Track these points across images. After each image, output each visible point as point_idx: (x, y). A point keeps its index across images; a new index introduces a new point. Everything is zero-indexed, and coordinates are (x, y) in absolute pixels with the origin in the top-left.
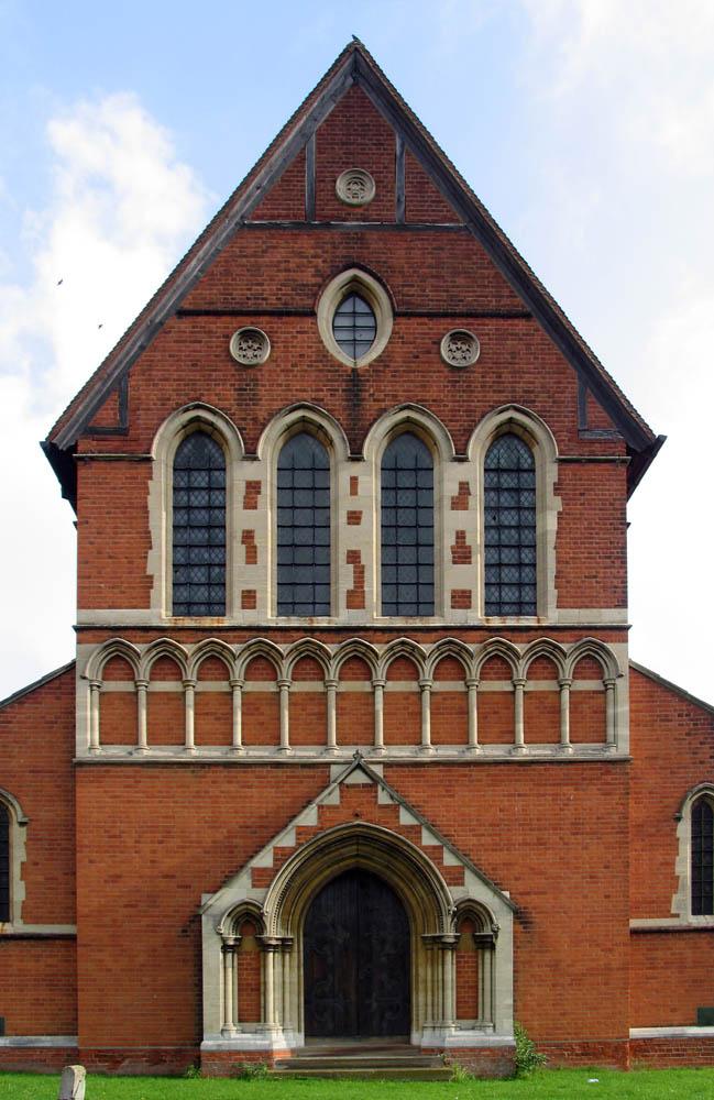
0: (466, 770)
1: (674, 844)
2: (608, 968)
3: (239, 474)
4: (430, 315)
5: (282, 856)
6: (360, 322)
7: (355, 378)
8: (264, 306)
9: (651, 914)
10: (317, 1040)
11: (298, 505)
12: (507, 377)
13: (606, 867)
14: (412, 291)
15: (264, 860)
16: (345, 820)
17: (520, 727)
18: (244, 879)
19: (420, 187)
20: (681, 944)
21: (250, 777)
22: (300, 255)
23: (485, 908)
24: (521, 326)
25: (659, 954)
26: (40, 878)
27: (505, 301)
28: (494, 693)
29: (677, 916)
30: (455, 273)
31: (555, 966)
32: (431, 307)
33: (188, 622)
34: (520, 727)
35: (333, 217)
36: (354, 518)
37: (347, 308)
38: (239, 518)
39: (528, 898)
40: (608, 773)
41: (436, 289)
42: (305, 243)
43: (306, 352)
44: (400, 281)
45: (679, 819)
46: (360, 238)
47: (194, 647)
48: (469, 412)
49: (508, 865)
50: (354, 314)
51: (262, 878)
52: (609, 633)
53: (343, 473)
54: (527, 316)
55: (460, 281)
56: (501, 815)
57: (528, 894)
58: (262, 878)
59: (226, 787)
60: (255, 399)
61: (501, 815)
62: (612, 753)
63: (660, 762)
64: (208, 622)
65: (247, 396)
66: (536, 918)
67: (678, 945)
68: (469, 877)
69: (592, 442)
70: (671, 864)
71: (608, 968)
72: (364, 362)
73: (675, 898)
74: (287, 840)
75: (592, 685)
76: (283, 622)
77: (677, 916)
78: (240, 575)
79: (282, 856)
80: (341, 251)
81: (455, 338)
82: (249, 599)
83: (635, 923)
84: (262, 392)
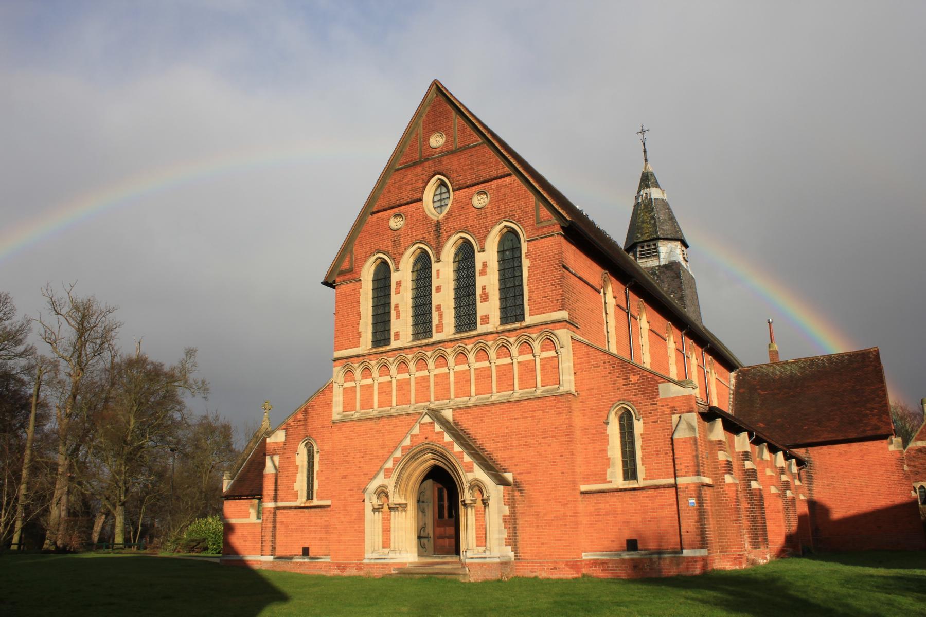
0: (489, 408)
2: (565, 516)
3: (479, 258)
4: (467, 187)
5: (396, 461)
6: (444, 196)
8: (403, 202)
9: (596, 482)
11: (661, 236)
12: (502, 206)
15: (389, 465)
16: (421, 440)
17: (516, 381)
18: (381, 475)
19: (463, 131)
21: (397, 422)
24: (508, 179)
25: (602, 506)
26: (323, 478)
29: (610, 482)
30: (478, 165)
31: (537, 514)
33: (508, 327)
34: (516, 381)
37: (438, 192)
38: (480, 281)
39: (523, 476)
44: (455, 175)
47: (515, 338)
49: (511, 458)
50: (441, 194)
51: (388, 473)
54: (509, 175)
55: (480, 168)
58: (388, 473)
59: (388, 427)
62: (562, 389)
63: (595, 391)
64: (516, 325)
65: (396, 243)
66: (526, 487)
67: (613, 499)
71: (565, 516)
74: (398, 454)
75: (552, 353)
77: (610, 482)
78: (482, 309)
79: (396, 461)
80: (433, 169)
81: (479, 193)
82: (486, 320)
83: (584, 488)
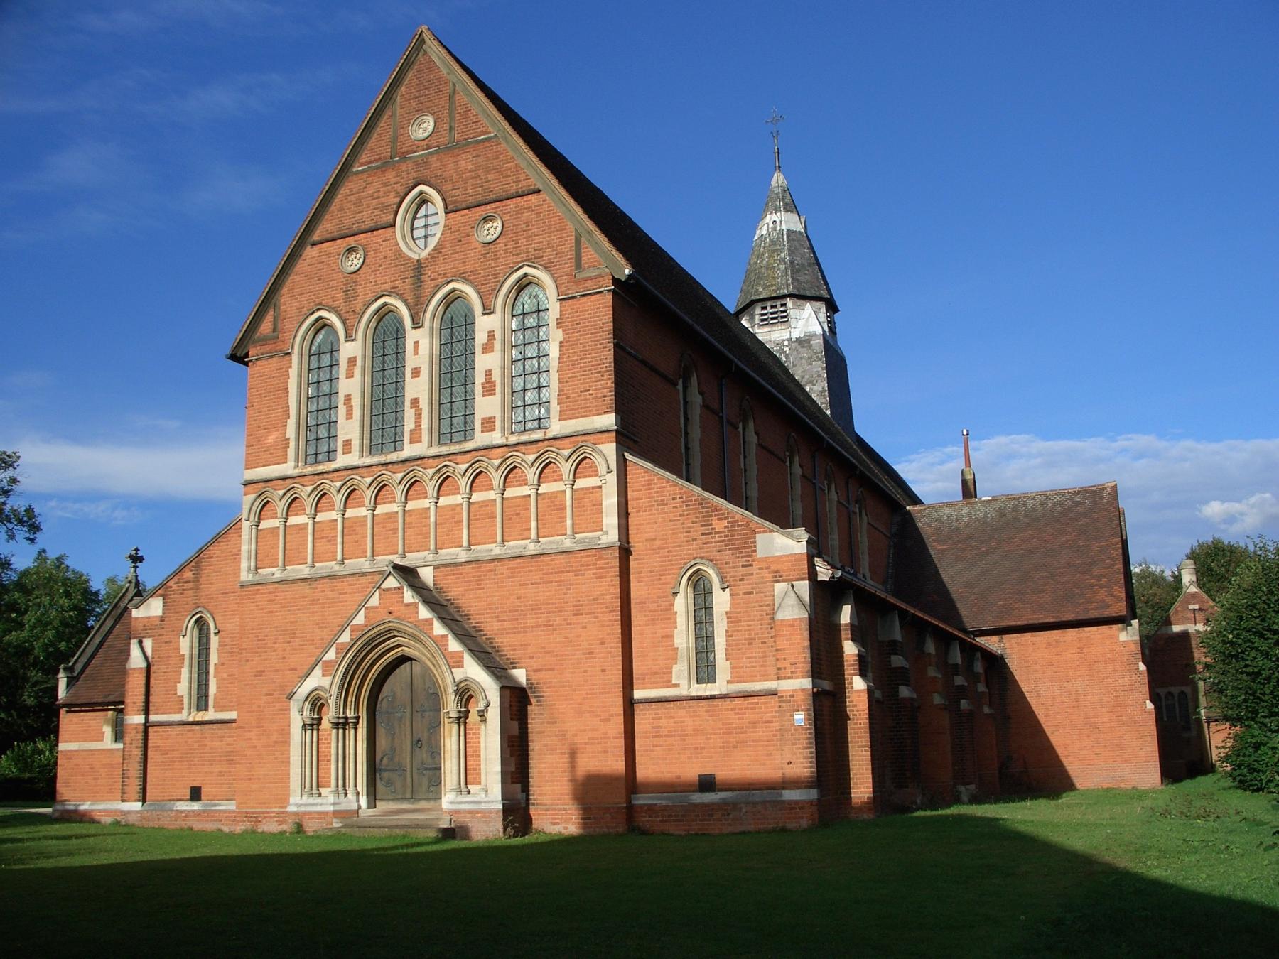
0: (490, 566)
1: (671, 619)
7: (419, 266)
8: (363, 227)
9: (656, 685)
10: (1021, 828)
12: (522, 242)
13: (603, 643)
14: (458, 192)
16: (382, 615)
20: (682, 712)
22: (386, 185)
23: (315, 690)
25: (663, 723)
27: (522, 184)
28: (516, 497)
29: (677, 685)
30: (488, 172)
32: (472, 200)
35: (409, 152)
36: (416, 372)
40: (601, 558)
41: (474, 186)
42: (390, 176)
43: (389, 254)
45: (675, 594)
46: (425, 162)
48: (496, 275)
49: (524, 646)
52: (599, 436)
53: (411, 335)
55: (491, 177)
56: (517, 602)
57: (539, 670)
59: (330, 595)
60: (355, 297)
61: (517, 602)
63: (658, 543)
67: (680, 712)
68: (468, 659)
69: (586, 280)
70: (671, 637)
72: (424, 254)
73: (675, 668)
76: (368, 460)
77: (677, 685)
80: (413, 175)
84: (360, 290)
